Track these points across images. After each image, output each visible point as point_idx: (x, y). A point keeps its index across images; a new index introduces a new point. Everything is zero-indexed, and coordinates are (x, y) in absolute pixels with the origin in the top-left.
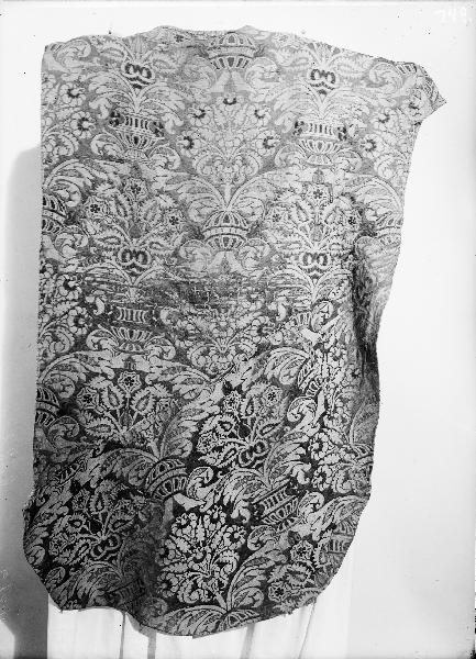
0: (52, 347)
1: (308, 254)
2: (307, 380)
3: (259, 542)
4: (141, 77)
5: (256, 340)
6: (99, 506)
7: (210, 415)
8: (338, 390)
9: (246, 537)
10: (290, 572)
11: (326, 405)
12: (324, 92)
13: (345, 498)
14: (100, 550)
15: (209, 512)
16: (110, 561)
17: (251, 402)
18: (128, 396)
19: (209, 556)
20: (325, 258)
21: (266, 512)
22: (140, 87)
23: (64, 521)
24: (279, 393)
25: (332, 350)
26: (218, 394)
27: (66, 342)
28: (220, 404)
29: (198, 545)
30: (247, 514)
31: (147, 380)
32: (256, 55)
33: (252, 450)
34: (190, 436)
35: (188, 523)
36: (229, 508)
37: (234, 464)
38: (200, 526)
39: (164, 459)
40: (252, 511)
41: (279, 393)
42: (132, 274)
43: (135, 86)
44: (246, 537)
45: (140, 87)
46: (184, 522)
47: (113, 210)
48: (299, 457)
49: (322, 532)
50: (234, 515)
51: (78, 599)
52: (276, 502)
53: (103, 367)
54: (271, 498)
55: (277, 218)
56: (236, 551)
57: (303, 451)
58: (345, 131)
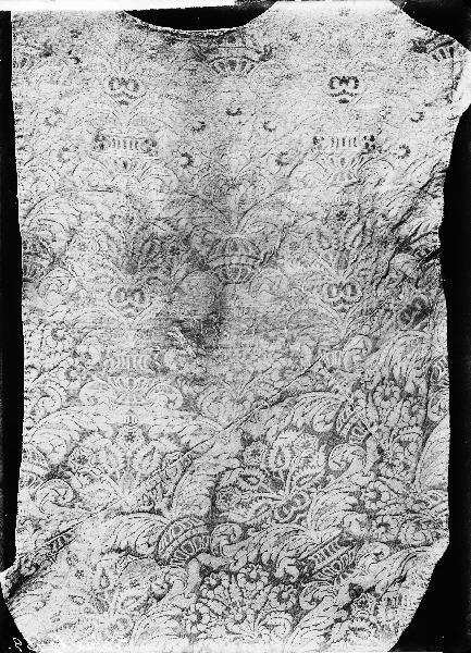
0: (40, 404)
1: (330, 285)
2: (348, 426)
3: (313, 599)
4: (126, 92)
5: (279, 385)
6: (280, 463)
7: (228, 469)
8: (394, 433)
9: (297, 596)
10: (353, 629)
11: (381, 451)
12: (344, 101)
13: (418, 549)
14: (286, 511)
15: (244, 571)
16: (299, 523)
17: (104, 575)
18: (129, 454)
19: (250, 618)
20: (353, 287)
21: (318, 566)
22: (127, 104)
23: (235, 475)
24: (314, 441)
25: (379, 389)
26: (235, 446)
27: (57, 397)
28: (240, 457)
29: (234, 604)
30: (294, 571)
31: (151, 435)
32: (262, 59)
33: (290, 504)
34: (206, 491)
35: (219, 582)
36: (271, 565)
37: (268, 521)
38: (233, 585)
39: (179, 519)
40: (300, 567)
41: (314, 441)
42: (129, 315)
43: (122, 102)
44: (297, 596)
45: (127, 104)
46: (213, 582)
47: (104, 245)
48: (350, 507)
49: (388, 585)
50: (279, 574)
51: (262, 564)
52: (331, 553)
53: (100, 423)
54: (322, 551)
55: (295, 246)
56: (286, 611)
57: (353, 500)
58: (372, 139)
